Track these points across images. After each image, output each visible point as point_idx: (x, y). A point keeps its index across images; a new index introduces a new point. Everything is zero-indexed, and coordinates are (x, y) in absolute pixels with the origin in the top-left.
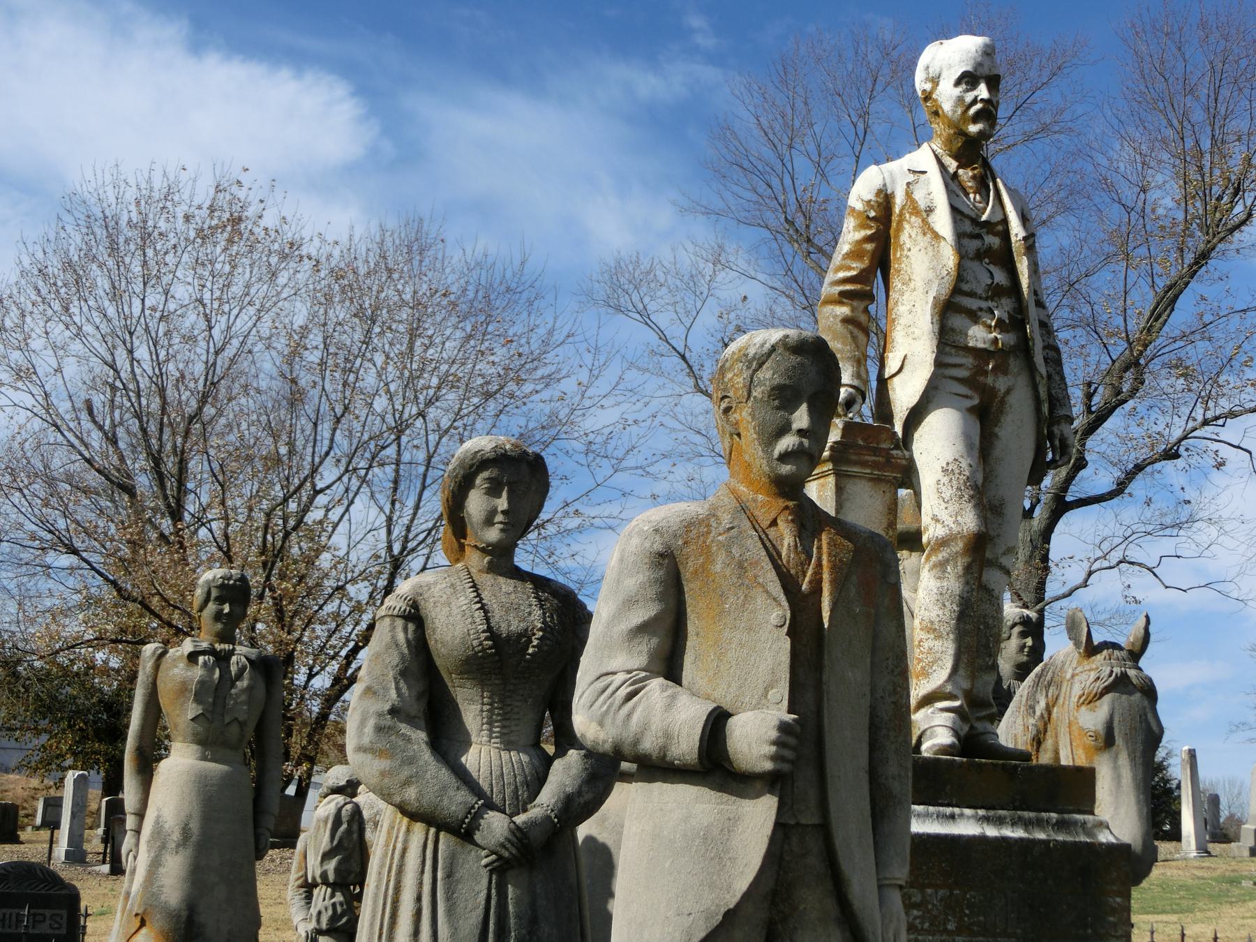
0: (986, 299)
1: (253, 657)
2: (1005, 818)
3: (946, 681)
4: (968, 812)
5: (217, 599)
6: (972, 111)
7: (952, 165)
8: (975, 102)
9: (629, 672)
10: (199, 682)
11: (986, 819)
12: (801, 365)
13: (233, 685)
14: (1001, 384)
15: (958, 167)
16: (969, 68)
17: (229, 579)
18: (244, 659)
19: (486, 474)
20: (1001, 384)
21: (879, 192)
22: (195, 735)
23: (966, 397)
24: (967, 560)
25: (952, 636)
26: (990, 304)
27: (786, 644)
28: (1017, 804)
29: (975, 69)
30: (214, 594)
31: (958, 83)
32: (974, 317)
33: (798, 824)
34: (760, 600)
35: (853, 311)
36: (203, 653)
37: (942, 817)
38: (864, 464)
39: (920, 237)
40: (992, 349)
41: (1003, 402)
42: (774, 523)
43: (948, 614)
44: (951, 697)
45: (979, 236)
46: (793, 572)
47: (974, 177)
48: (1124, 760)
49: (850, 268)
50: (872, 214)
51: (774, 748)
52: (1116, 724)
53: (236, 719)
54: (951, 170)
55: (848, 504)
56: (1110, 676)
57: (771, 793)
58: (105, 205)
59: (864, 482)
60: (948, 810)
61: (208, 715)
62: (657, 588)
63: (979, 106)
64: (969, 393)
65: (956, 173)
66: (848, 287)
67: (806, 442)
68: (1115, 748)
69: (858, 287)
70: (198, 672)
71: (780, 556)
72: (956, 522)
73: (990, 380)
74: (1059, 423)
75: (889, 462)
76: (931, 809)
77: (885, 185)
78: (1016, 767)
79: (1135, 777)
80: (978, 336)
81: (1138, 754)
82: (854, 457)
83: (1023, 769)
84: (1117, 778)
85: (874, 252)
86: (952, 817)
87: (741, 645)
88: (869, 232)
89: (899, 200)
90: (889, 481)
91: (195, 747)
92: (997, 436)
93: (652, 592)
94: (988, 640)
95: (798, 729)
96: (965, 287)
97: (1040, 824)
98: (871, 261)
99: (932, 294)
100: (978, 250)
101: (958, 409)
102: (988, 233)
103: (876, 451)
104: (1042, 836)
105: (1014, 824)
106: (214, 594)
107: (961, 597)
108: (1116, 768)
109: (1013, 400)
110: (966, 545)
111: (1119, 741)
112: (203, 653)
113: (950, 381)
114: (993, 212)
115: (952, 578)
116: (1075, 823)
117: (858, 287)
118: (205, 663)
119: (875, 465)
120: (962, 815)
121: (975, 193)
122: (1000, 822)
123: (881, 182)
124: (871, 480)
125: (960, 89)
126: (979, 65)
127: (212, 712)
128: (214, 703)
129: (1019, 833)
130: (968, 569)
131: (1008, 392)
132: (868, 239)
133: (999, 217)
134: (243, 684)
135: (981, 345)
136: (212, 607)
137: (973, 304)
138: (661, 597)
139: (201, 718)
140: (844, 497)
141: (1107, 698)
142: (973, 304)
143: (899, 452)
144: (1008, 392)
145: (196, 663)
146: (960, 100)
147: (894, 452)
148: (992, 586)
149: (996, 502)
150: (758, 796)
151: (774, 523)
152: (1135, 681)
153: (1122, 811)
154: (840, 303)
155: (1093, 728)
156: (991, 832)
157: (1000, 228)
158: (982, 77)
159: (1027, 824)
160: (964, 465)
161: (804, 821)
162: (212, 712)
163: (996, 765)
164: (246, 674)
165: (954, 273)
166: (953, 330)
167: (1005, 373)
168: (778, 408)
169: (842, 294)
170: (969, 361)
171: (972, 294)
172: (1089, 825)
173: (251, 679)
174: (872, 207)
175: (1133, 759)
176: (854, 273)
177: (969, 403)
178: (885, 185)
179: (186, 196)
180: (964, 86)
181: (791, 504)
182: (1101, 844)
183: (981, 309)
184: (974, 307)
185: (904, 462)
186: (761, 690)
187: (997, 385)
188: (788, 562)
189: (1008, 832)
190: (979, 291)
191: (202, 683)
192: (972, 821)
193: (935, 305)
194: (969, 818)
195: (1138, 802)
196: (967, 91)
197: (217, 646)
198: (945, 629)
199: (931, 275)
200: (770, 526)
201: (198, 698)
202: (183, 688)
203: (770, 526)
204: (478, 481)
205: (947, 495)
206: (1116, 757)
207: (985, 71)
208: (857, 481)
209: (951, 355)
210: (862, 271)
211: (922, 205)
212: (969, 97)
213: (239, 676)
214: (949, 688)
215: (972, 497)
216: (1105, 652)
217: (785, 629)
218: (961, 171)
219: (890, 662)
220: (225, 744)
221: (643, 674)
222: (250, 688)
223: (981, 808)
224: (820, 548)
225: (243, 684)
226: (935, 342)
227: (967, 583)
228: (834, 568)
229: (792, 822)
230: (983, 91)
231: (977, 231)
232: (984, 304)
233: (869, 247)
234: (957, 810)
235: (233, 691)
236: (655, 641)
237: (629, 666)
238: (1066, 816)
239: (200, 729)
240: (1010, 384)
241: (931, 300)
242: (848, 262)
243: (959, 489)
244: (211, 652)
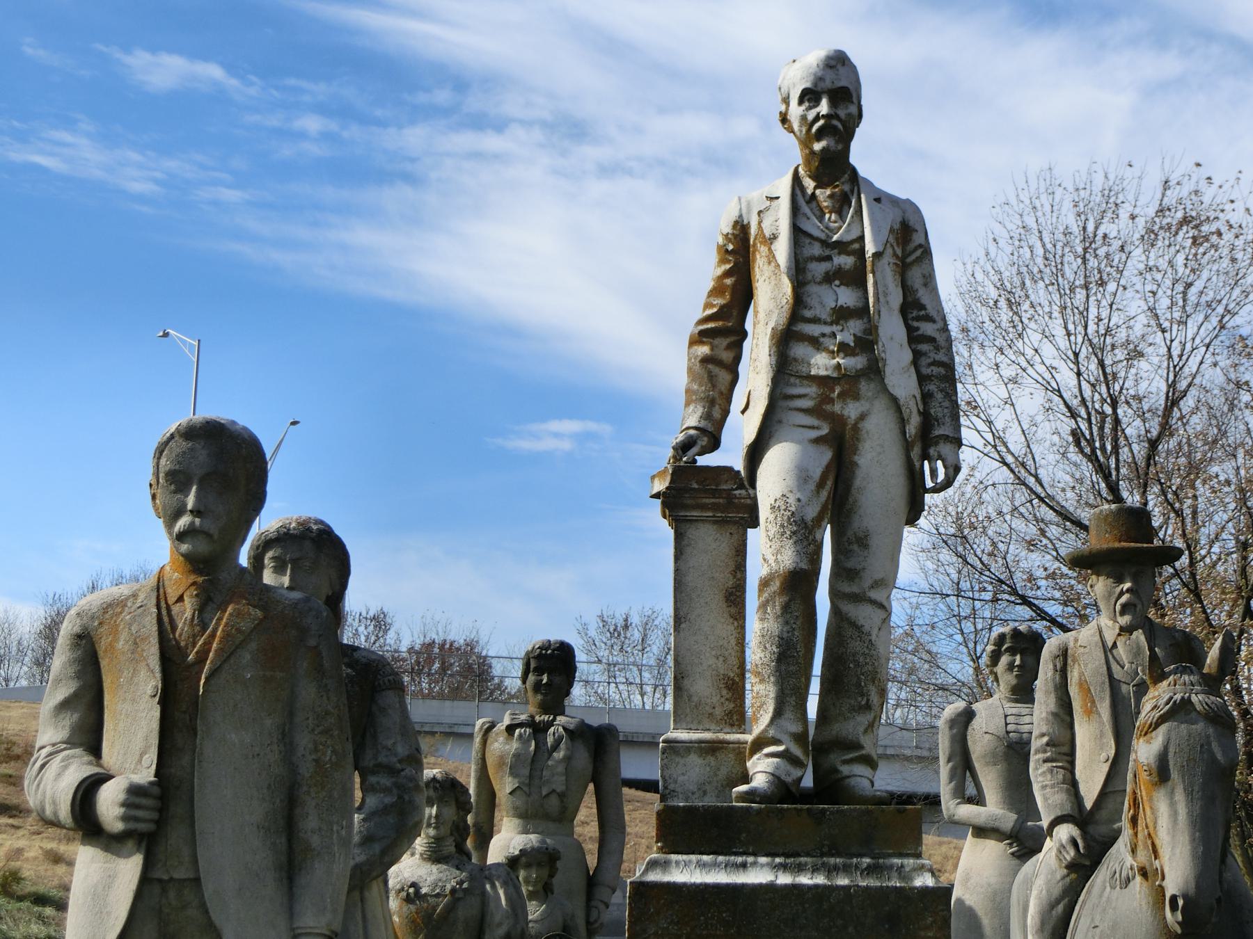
0: (831, 324)
1: (571, 727)
2: (806, 864)
3: (768, 726)
4: (763, 860)
5: (536, 670)
6: (814, 129)
7: (809, 184)
8: (817, 118)
9: (53, 745)
10: (514, 755)
11: (784, 867)
12: (192, 449)
13: (550, 754)
14: (851, 410)
15: (816, 188)
16: (808, 85)
17: (547, 649)
18: (561, 729)
19: (270, 554)
20: (851, 410)
21: (736, 223)
22: (515, 808)
23: (812, 427)
24: (785, 599)
25: (772, 679)
26: (835, 328)
27: (156, 713)
28: (825, 850)
29: (815, 84)
30: (533, 665)
31: (801, 102)
32: (816, 343)
33: (171, 879)
34: (143, 673)
35: (712, 349)
36: (520, 725)
37: (702, 866)
38: (703, 507)
39: (766, 267)
40: (835, 375)
41: (856, 428)
42: (181, 599)
43: (768, 655)
44: (776, 742)
45: (829, 258)
46: (183, 644)
47: (831, 196)
48: (1180, 796)
49: (712, 306)
50: (731, 247)
51: (122, 810)
52: (1171, 755)
53: (554, 791)
54: (809, 191)
55: (688, 550)
56: (1167, 703)
57: (138, 850)
58: (1039, 214)
59: (707, 526)
60: (740, 859)
61: (526, 789)
62: (75, 667)
63: (821, 122)
64: (815, 422)
65: (813, 194)
66: (710, 325)
67: (197, 521)
68: (1170, 783)
69: (719, 324)
70: (515, 745)
71: (174, 628)
72: (776, 560)
73: (837, 408)
74: (937, 444)
75: (731, 502)
76: (721, 858)
77: (741, 216)
78: (823, 811)
79: (1190, 813)
80: (821, 363)
81: (1196, 788)
82: (689, 502)
83: (832, 813)
84: (1174, 814)
85: (734, 285)
86: (744, 866)
87: (127, 716)
88: (728, 266)
89: (753, 230)
90: (735, 523)
91: (516, 821)
92: (856, 464)
93: (71, 671)
94: (859, 678)
95: (156, 790)
96: (808, 314)
97: (846, 869)
98: (732, 295)
99: (772, 324)
100: (827, 273)
101: (792, 441)
102: (839, 254)
103: (715, 493)
104: (843, 881)
105: (815, 870)
106: (533, 665)
107: (781, 638)
108: (1173, 805)
109: (869, 425)
110: (782, 584)
111: (1174, 774)
112: (520, 725)
113: (796, 413)
114: (848, 231)
115: (771, 617)
116: (891, 867)
117: (719, 324)
118: (520, 735)
119: (715, 508)
120: (754, 864)
121: (830, 213)
122: (800, 869)
123: (737, 214)
124: (715, 522)
125: (803, 107)
126: (819, 79)
127: (529, 785)
128: (531, 777)
129: (820, 880)
130: (786, 608)
131: (862, 417)
132: (727, 274)
133: (854, 235)
134: (560, 754)
135: (823, 373)
136: (1005, 660)
137: (814, 330)
138: (79, 675)
139: (518, 792)
140: (685, 542)
141: (1163, 728)
142: (814, 330)
143: (743, 492)
144: (862, 417)
145: (512, 735)
146: (804, 118)
147: (737, 492)
148: (861, 622)
149: (861, 534)
150: (129, 856)
151: (181, 599)
152: (1199, 707)
153: (1178, 851)
154: (701, 343)
155: (1146, 762)
156: (784, 879)
157: (856, 246)
158: (823, 92)
159: (831, 871)
160: (792, 500)
161: (176, 876)
162: (529, 785)
163: (801, 810)
164: (562, 745)
165: (791, 301)
166: (795, 360)
167: (856, 397)
168: (175, 492)
169: (702, 333)
170: (812, 390)
171: (815, 320)
172: (907, 869)
173: (567, 749)
174: (730, 241)
175: (1189, 793)
176: (715, 310)
177: (814, 434)
178: (741, 216)
179: (1131, 197)
180: (807, 104)
181: (200, 579)
182: (916, 888)
183: (824, 335)
184: (816, 334)
185: (749, 501)
186: (137, 757)
187: (846, 413)
188: (181, 635)
189: (805, 880)
190: (824, 316)
191: (517, 756)
192: (766, 869)
193: (772, 337)
194: (762, 866)
195: (1193, 840)
196: (810, 108)
197: (537, 718)
198: (766, 672)
199: (772, 305)
200: (177, 602)
201: (513, 773)
202: (502, 758)
203: (177, 602)
204: (266, 561)
205: (771, 534)
206: (1172, 792)
207: (828, 84)
208: (701, 525)
209: (795, 385)
210: (722, 307)
211: (767, 233)
212: (811, 115)
213: (556, 747)
214: (771, 733)
215: (794, 533)
216: (1171, 678)
217: (157, 699)
218: (818, 192)
219: (310, 721)
220: (547, 817)
221: (64, 746)
222: (568, 759)
223: (778, 855)
224: (220, 619)
225: (560, 754)
226: (771, 375)
227: (787, 623)
228: (227, 636)
229: (165, 877)
230: (824, 107)
231: (827, 252)
232: (827, 330)
233: (729, 281)
234: (750, 859)
235: (550, 763)
236: (76, 716)
237: (54, 740)
238: (881, 861)
239: (518, 803)
240: (864, 409)
241: (769, 331)
242: (711, 299)
243: (782, 526)
244: (531, 723)
